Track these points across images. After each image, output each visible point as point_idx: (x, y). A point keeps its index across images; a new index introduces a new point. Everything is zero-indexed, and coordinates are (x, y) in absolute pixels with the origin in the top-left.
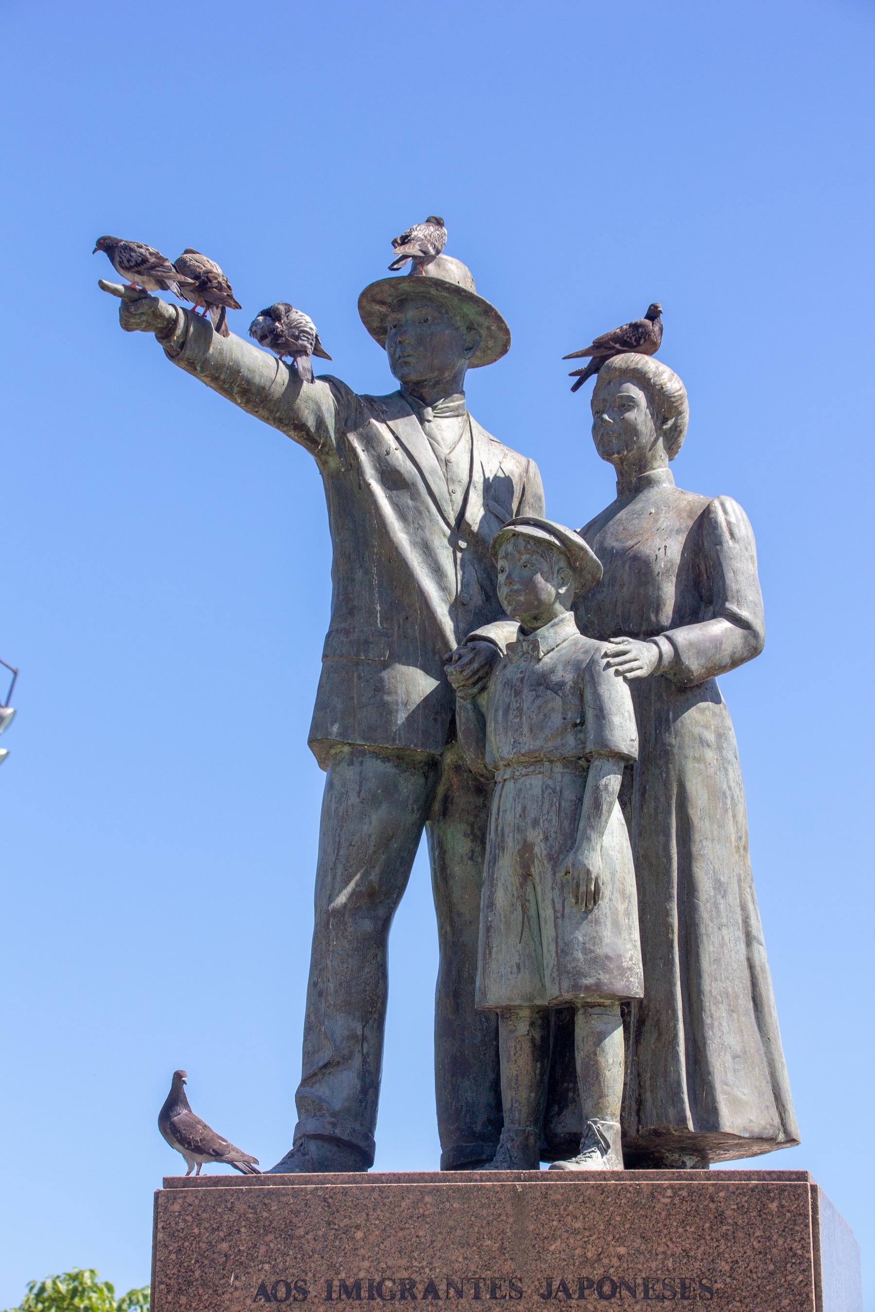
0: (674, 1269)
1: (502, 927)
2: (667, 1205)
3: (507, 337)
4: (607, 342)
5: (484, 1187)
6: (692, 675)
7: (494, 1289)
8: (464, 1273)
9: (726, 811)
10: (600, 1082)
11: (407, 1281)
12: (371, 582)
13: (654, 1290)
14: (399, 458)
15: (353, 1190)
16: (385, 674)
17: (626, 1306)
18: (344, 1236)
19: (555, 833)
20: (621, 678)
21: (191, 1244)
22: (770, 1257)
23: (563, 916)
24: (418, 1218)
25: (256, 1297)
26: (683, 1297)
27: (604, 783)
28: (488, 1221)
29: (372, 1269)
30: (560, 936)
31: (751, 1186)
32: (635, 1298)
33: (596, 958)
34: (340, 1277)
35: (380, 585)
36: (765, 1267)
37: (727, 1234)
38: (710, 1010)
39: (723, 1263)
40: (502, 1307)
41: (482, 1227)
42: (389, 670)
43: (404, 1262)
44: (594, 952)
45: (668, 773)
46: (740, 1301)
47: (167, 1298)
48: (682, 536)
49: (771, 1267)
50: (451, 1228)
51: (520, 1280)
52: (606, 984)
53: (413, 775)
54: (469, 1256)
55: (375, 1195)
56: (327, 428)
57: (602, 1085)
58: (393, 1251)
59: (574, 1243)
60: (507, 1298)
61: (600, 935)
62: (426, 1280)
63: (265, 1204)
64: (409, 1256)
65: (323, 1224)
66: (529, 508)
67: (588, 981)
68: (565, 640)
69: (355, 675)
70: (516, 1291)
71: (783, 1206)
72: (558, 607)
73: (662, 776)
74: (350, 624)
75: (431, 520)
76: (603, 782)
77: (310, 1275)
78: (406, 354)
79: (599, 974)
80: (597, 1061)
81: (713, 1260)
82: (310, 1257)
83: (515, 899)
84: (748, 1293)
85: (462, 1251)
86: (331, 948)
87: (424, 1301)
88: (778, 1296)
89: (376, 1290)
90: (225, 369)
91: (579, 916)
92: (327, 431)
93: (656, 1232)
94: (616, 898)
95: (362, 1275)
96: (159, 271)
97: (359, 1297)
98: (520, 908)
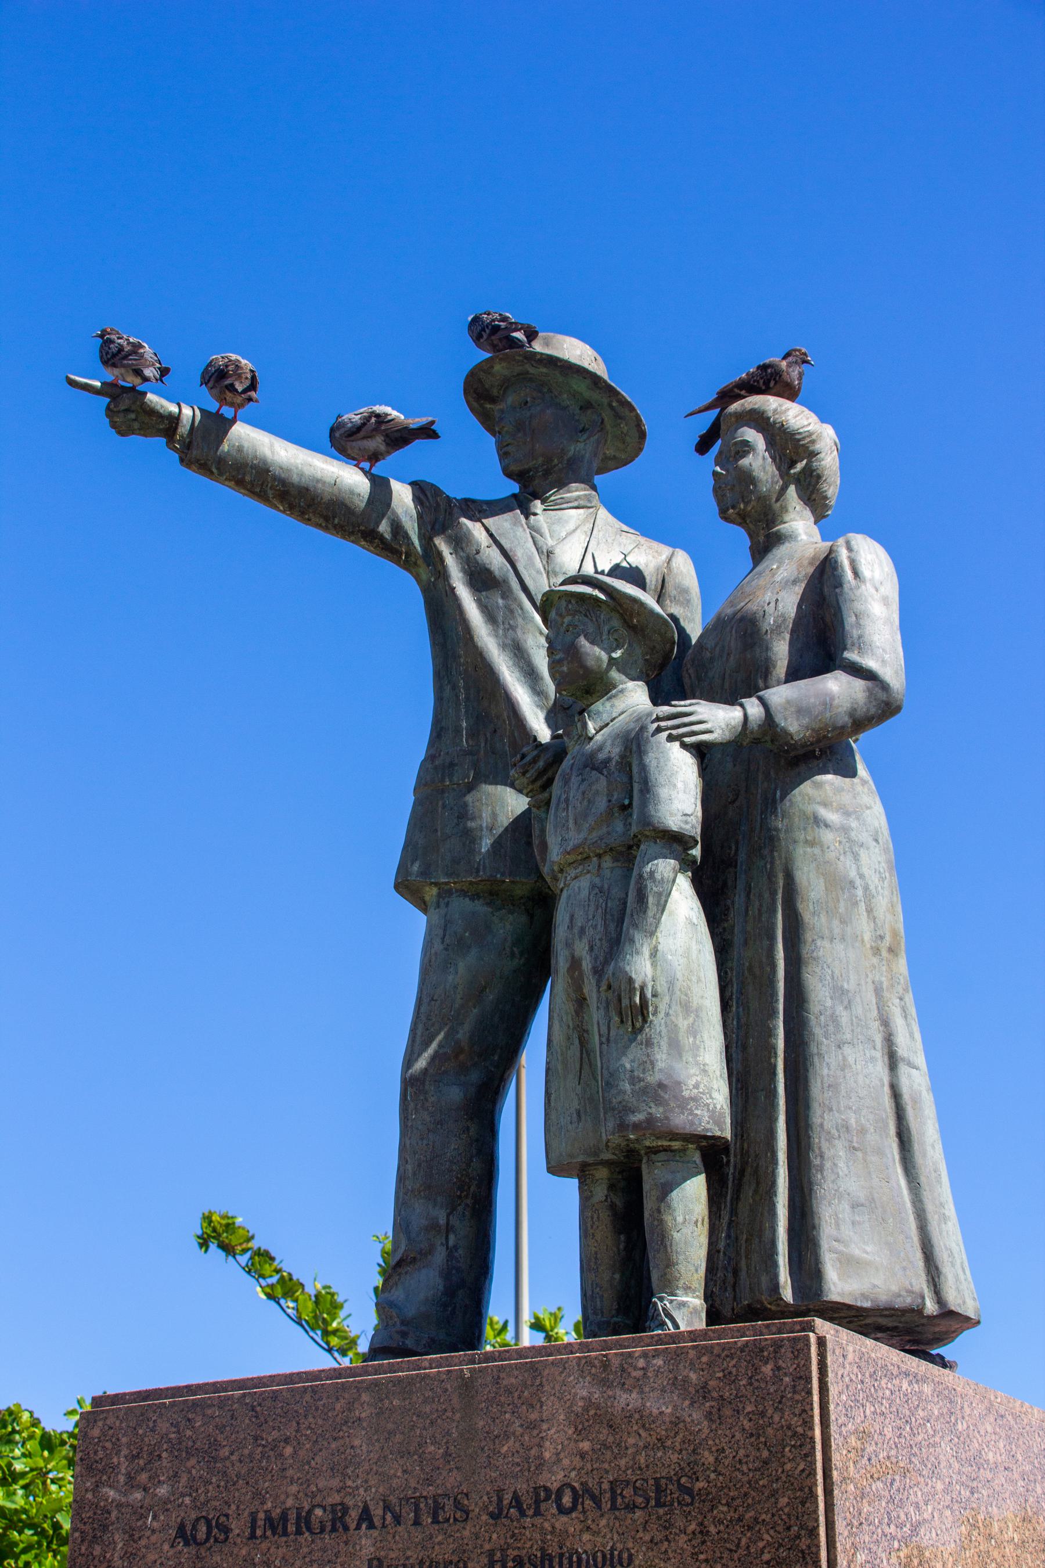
0: (647, 1466)
1: (560, 1067)
2: (638, 1380)
3: (634, 413)
4: (731, 390)
5: (427, 1376)
6: (792, 738)
7: (436, 1510)
8: (403, 1491)
9: (856, 904)
10: (666, 1247)
11: (339, 1507)
12: (457, 697)
13: (623, 1497)
14: (494, 559)
15: (284, 1393)
16: (469, 798)
17: (589, 1522)
18: (271, 1453)
19: (601, 940)
20: (677, 744)
21: (109, 1478)
22: (763, 1440)
23: (608, 1040)
24: (353, 1423)
25: (174, 1541)
26: (659, 1504)
27: (649, 870)
28: (431, 1420)
29: (301, 1494)
30: (605, 1066)
31: (739, 1344)
32: (601, 1510)
33: (646, 1087)
34: (265, 1508)
35: (467, 699)
36: (758, 1454)
37: (711, 1413)
38: (820, 1148)
39: (706, 1453)
40: (445, 1534)
41: (425, 1428)
42: (474, 792)
43: (335, 1483)
44: (643, 1081)
45: (772, 863)
46: (728, 1504)
47: (80, 1549)
48: (800, 586)
49: (765, 1454)
50: (390, 1433)
51: (467, 1495)
52: (657, 1120)
53: (511, 912)
54: (410, 1468)
55: (307, 1397)
56: (406, 533)
57: (669, 1250)
58: (324, 1469)
59: (530, 1440)
60: (452, 1520)
61: (652, 1059)
62: (360, 1504)
63: (189, 1420)
64: (342, 1473)
65: (250, 1440)
66: (671, 601)
67: (638, 1117)
68: (622, 713)
69: (440, 803)
70: (461, 1510)
71: (779, 1368)
72: (614, 674)
73: (766, 868)
74: (437, 748)
75: (524, 618)
76: (648, 868)
77: (233, 1507)
78: (505, 444)
79: (650, 1107)
80: (662, 1220)
81: (694, 1450)
82: (234, 1485)
83: (571, 1031)
84: (736, 1493)
85: (401, 1462)
86: (410, 1124)
87: (357, 1532)
88: (774, 1493)
89: (304, 1522)
90: (249, 469)
91: (626, 1038)
92: (407, 536)
93: (626, 1417)
94: (675, 1012)
95: (290, 1502)
96: (131, 360)
97: (285, 1533)
98: (577, 1042)
